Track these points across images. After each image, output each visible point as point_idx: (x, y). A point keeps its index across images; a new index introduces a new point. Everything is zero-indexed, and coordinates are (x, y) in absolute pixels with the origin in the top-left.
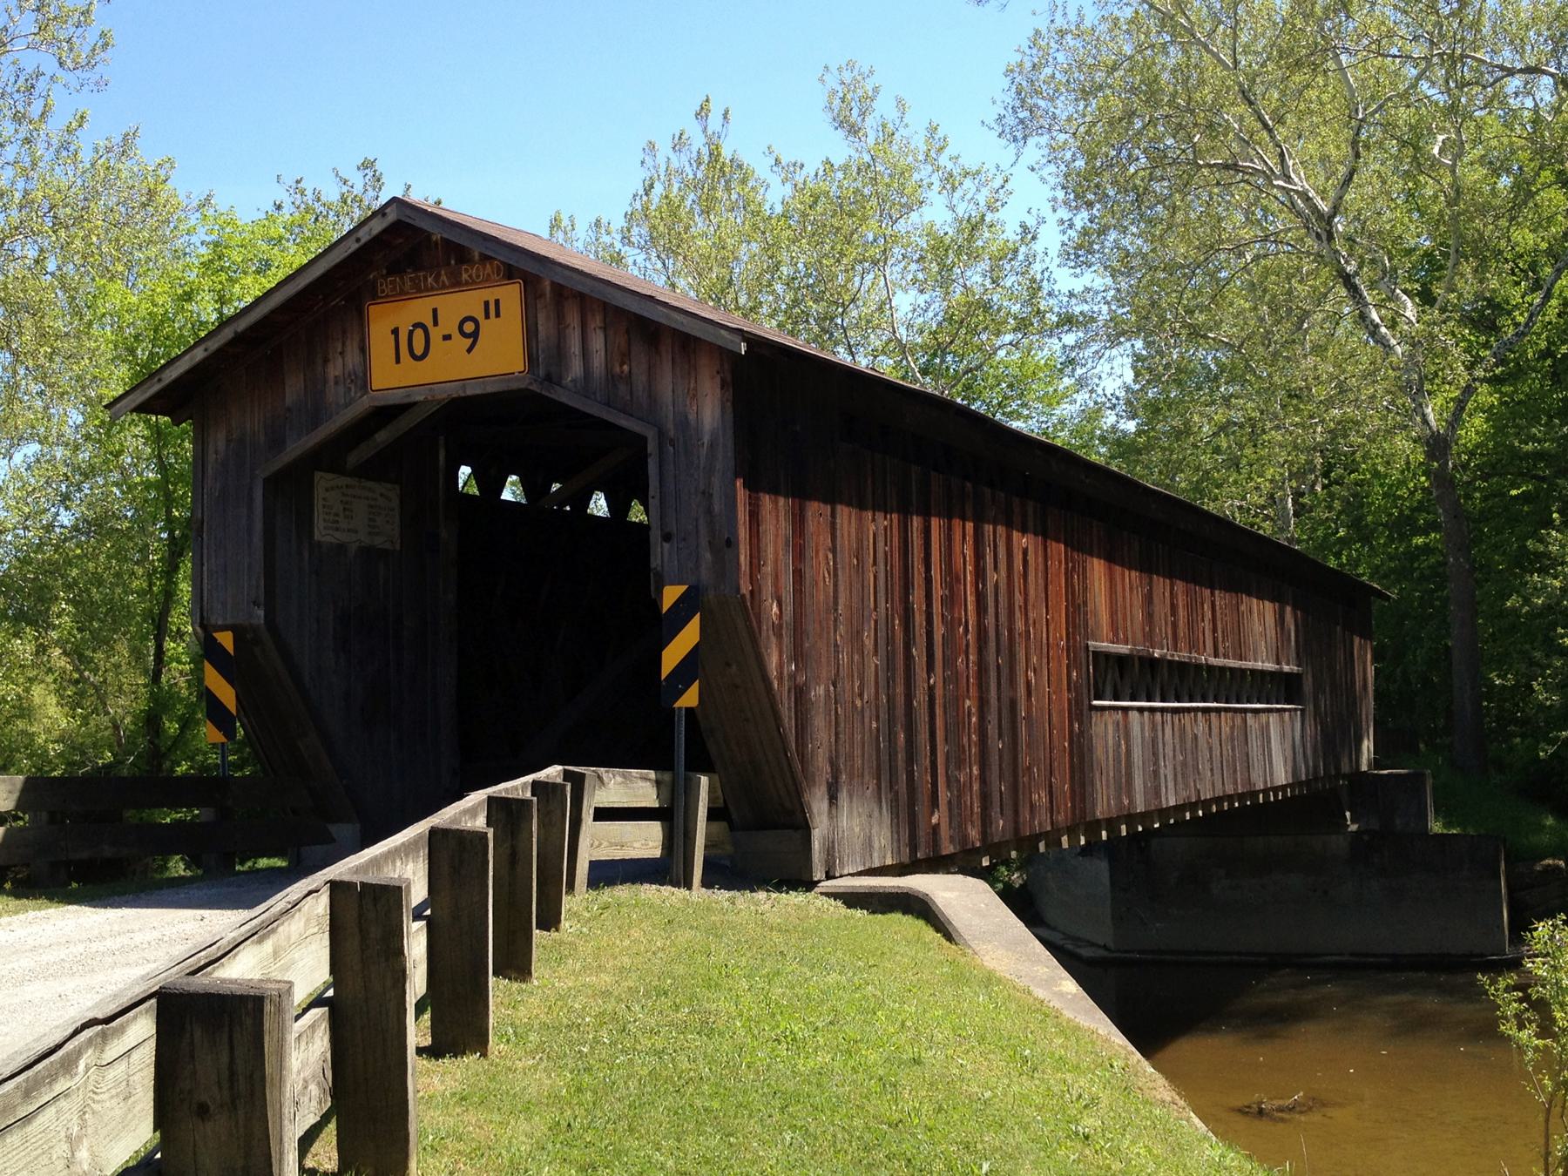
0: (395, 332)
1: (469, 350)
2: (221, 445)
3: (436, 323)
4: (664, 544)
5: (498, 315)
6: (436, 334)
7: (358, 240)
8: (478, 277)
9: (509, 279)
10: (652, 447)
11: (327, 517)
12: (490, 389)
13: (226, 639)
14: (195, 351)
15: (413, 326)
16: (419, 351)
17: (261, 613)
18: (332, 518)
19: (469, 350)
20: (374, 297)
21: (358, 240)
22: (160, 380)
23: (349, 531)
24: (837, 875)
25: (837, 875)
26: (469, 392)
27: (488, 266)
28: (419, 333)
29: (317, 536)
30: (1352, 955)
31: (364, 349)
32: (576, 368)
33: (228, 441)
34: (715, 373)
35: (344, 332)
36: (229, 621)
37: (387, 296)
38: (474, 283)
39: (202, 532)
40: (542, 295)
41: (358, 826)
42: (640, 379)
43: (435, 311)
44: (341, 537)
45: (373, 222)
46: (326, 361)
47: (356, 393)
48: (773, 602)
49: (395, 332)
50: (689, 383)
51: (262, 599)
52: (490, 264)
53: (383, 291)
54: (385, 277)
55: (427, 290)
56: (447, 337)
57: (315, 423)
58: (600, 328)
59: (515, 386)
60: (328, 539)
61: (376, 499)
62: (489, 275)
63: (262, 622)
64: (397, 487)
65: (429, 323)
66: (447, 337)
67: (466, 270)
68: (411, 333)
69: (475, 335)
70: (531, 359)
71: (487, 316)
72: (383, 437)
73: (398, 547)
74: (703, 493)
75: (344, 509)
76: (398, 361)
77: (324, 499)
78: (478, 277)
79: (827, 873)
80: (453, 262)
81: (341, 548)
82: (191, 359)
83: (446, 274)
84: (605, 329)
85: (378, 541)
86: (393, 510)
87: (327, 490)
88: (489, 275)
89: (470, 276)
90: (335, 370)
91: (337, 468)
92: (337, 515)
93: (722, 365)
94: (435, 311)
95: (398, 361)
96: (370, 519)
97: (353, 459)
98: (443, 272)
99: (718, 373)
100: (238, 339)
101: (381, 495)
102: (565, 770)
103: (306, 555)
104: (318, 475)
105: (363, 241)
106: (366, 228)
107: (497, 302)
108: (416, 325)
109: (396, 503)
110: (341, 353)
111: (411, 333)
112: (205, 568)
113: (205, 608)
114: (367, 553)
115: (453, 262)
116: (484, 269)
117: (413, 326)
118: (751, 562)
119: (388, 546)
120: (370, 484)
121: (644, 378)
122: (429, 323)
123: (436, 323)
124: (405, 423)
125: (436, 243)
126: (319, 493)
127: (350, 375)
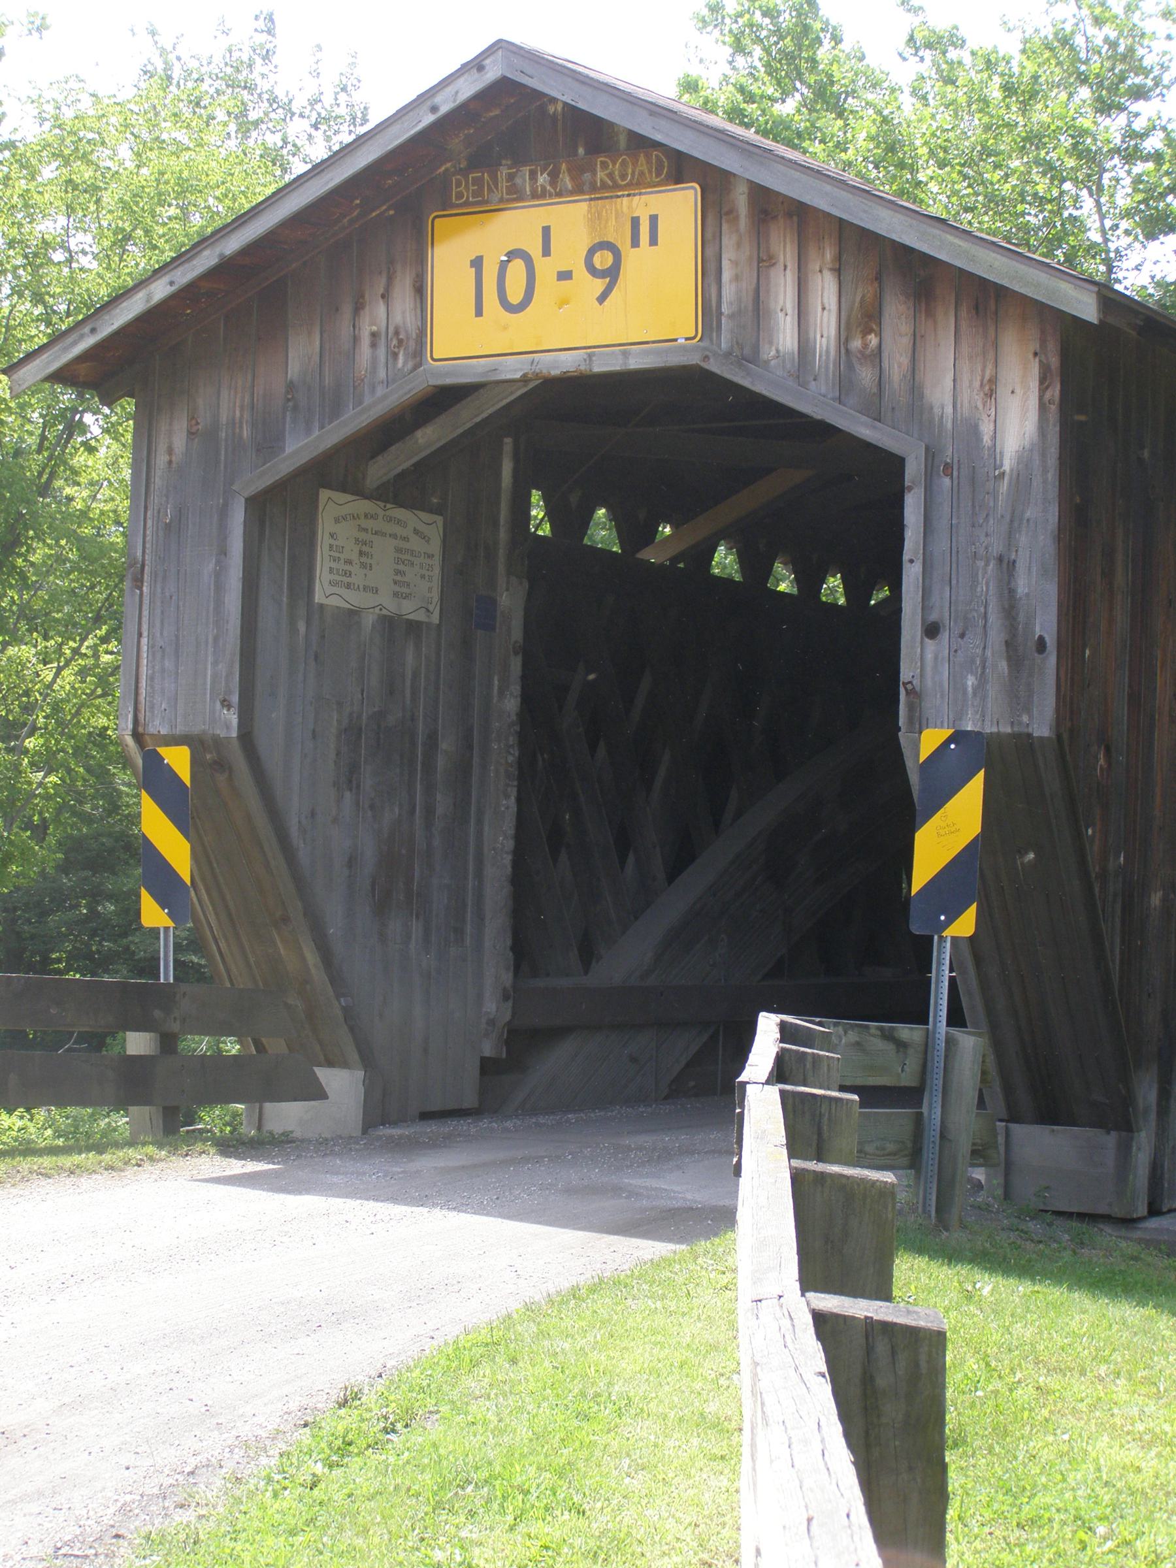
0: (477, 263)
1: (602, 298)
2: (179, 442)
3: (546, 252)
4: (927, 640)
5: (654, 241)
6: (546, 269)
7: (434, 109)
8: (623, 177)
9: (677, 183)
10: (913, 470)
11: (333, 565)
12: (634, 364)
13: (178, 759)
14: (153, 286)
15: (507, 254)
16: (515, 297)
17: (233, 718)
18: (341, 566)
19: (602, 298)
20: (445, 204)
21: (434, 109)
22: (93, 331)
23: (365, 588)
24: (1165, 1210)
25: (1165, 1210)
26: (598, 368)
27: (642, 159)
28: (517, 268)
29: (318, 597)
30: (629, 1149)
31: (420, 290)
32: (786, 337)
33: (191, 434)
34: (1031, 356)
35: (391, 262)
36: (180, 730)
37: (467, 204)
38: (616, 187)
39: (142, 582)
40: (732, 212)
41: (360, 1074)
42: (897, 362)
43: (546, 231)
44: (355, 599)
45: (462, 80)
46: (358, 308)
47: (405, 363)
48: (1099, 747)
49: (477, 263)
50: (983, 370)
51: (235, 699)
52: (648, 157)
53: (460, 196)
54: (465, 172)
55: (535, 196)
56: (565, 276)
57: (335, 407)
58: (831, 269)
59: (675, 360)
60: (334, 601)
61: (406, 539)
62: (642, 173)
63: (234, 734)
64: (439, 519)
65: (535, 251)
66: (565, 276)
67: (604, 165)
68: (503, 266)
69: (612, 274)
70: (709, 314)
71: (635, 243)
72: (429, 437)
73: (435, 618)
74: (1000, 559)
75: (361, 553)
76: (479, 312)
77: (332, 535)
78: (623, 177)
79: (1150, 1205)
80: (581, 151)
81: (353, 614)
82: (149, 297)
83: (569, 170)
84: (838, 271)
85: (409, 609)
86: (431, 556)
87: (337, 520)
88: (642, 173)
89: (611, 176)
90: (376, 317)
91: (351, 486)
92: (349, 562)
93: (1043, 342)
94: (546, 231)
95: (479, 312)
96: (398, 572)
97: (379, 471)
98: (564, 166)
99: (1036, 354)
100: (225, 269)
101: (416, 531)
102: (782, 1022)
103: (302, 627)
104: (324, 494)
105: (444, 109)
106: (449, 90)
107: (654, 219)
108: (512, 255)
109: (435, 547)
110: (383, 296)
111: (503, 266)
112: (144, 641)
113: (142, 707)
114: (390, 625)
115: (581, 151)
116: (635, 165)
117: (507, 254)
118: (1072, 679)
119: (421, 616)
120: (400, 513)
121: (905, 360)
122: (535, 251)
123: (546, 252)
124: (466, 416)
125: (554, 117)
126: (325, 525)
127: (397, 333)
